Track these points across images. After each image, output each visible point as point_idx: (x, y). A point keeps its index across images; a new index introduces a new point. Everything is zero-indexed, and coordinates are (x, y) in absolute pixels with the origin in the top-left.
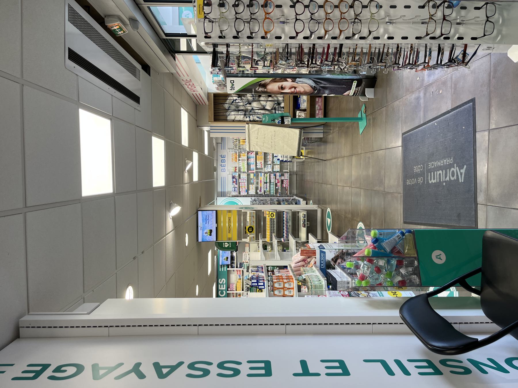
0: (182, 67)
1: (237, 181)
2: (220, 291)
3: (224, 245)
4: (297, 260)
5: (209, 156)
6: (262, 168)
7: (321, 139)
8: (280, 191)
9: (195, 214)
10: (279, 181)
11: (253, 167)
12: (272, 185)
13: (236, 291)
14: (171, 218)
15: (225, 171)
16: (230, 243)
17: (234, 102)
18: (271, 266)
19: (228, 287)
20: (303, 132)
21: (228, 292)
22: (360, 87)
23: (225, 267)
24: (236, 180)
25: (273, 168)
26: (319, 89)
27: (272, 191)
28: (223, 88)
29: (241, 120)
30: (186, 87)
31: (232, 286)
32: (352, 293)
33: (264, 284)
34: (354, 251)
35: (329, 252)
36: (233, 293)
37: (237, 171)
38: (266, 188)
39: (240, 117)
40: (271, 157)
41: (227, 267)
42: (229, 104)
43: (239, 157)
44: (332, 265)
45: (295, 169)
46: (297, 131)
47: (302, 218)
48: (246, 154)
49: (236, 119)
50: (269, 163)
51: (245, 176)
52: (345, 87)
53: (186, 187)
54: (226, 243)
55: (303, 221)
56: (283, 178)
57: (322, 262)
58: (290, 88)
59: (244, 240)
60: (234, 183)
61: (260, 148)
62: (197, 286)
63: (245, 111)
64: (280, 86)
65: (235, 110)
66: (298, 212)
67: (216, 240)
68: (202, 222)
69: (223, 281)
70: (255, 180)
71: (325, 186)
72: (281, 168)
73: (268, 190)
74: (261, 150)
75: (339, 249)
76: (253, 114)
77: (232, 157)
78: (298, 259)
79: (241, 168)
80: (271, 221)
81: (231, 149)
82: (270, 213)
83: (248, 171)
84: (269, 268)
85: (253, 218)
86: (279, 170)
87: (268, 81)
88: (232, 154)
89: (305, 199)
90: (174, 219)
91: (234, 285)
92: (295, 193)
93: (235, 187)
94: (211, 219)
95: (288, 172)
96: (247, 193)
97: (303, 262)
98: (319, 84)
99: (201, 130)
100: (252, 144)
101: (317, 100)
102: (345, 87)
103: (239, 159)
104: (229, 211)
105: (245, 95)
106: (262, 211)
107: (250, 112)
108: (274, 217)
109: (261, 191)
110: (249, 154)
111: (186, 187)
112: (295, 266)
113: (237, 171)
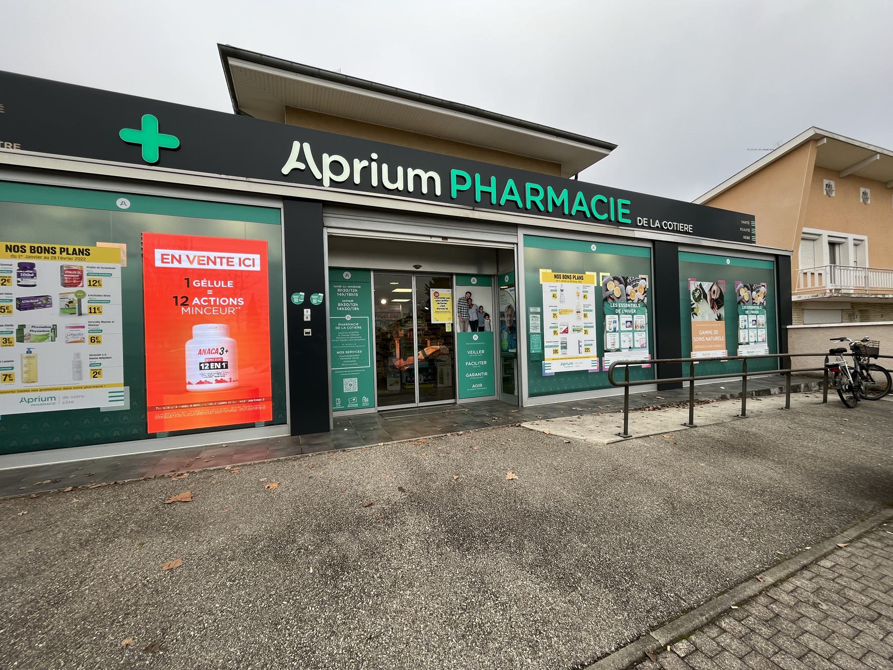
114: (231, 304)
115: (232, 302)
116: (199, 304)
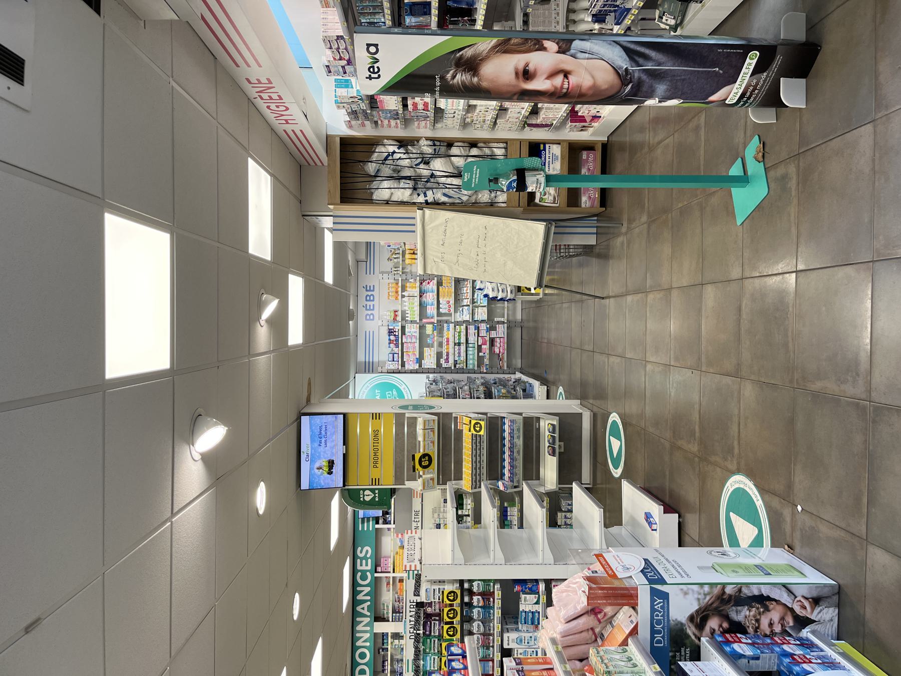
0: (253, 55)
1: (397, 340)
2: (359, 574)
3: (362, 496)
4: (572, 612)
5: (335, 288)
6: (451, 314)
7: (588, 250)
8: (486, 361)
9: (293, 422)
10: (486, 341)
11: (431, 310)
12: (471, 349)
13: (394, 572)
14: (197, 457)
15: (373, 320)
16: (377, 492)
17: (390, 158)
18: (479, 580)
19: (377, 565)
20: (553, 229)
21: (376, 575)
22: (765, 74)
23: (371, 523)
24: (395, 337)
25: (473, 314)
26: (639, 78)
27: (471, 362)
28: (363, 125)
29: (405, 200)
30: (262, 105)
35: (681, 595)
36: (386, 577)
37: (399, 318)
38: (459, 356)
39: (403, 194)
40: (470, 291)
41: (375, 522)
42: (376, 162)
43: (403, 289)
44: (688, 636)
45: (519, 317)
46: (540, 227)
47: (547, 433)
48: (418, 284)
49: (392, 199)
50: (465, 302)
51: (415, 330)
52: (721, 72)
53: (263, 364)
54: (367, 492)
55: (551, 441)
56: (493, 334)
57: (658, 627)
58: (552, 75)
59: (409, 484)
60: (391, 345)
61: (451, 269)
62: (297, 595)
63: (414, 180)
64: (521, 67)
65: (391, 178)
66: (538, 419)
67: (344, 485)
68: (309, 443)
69: (367, 551)
70: (436, 338)
71: (604, 358)
72: (490, 313)
73: (462, 359)
74: (449, 272)
75: (712, 585)
76: (434, 187)
77: (389, 290)
78: (575, 607)
79: (407, 312)
80: (474, 441)
81: (386, 272)
82: (473, 422)
83: (421, 320)
85: (430, 350)
86: (485, 317)
87: (485, 47)
88: (389, 284)
89: (544, 381)
90: (208, 459)
91: (390, 559)
92: (519, 366)
93: (393, 352)
94: (332, 434)
95: (503, 323)
96: (418, 364)
97: (592, 617)
98: (641, 61)
99: (315, 228)
100: (430, 258)
101: (584, 156)
102: (721, 72)
103: (403, 293)
104: (374, 415)
105: (416, 142)
106: (454, 415)
107: (427, 182)
108: (482, 433)
109: (447, 360)
110: (424, 284)
111: (263, 364)
112: (565, 631)
113: (399, 318)
114: (358, 589)
116: (369, 603)
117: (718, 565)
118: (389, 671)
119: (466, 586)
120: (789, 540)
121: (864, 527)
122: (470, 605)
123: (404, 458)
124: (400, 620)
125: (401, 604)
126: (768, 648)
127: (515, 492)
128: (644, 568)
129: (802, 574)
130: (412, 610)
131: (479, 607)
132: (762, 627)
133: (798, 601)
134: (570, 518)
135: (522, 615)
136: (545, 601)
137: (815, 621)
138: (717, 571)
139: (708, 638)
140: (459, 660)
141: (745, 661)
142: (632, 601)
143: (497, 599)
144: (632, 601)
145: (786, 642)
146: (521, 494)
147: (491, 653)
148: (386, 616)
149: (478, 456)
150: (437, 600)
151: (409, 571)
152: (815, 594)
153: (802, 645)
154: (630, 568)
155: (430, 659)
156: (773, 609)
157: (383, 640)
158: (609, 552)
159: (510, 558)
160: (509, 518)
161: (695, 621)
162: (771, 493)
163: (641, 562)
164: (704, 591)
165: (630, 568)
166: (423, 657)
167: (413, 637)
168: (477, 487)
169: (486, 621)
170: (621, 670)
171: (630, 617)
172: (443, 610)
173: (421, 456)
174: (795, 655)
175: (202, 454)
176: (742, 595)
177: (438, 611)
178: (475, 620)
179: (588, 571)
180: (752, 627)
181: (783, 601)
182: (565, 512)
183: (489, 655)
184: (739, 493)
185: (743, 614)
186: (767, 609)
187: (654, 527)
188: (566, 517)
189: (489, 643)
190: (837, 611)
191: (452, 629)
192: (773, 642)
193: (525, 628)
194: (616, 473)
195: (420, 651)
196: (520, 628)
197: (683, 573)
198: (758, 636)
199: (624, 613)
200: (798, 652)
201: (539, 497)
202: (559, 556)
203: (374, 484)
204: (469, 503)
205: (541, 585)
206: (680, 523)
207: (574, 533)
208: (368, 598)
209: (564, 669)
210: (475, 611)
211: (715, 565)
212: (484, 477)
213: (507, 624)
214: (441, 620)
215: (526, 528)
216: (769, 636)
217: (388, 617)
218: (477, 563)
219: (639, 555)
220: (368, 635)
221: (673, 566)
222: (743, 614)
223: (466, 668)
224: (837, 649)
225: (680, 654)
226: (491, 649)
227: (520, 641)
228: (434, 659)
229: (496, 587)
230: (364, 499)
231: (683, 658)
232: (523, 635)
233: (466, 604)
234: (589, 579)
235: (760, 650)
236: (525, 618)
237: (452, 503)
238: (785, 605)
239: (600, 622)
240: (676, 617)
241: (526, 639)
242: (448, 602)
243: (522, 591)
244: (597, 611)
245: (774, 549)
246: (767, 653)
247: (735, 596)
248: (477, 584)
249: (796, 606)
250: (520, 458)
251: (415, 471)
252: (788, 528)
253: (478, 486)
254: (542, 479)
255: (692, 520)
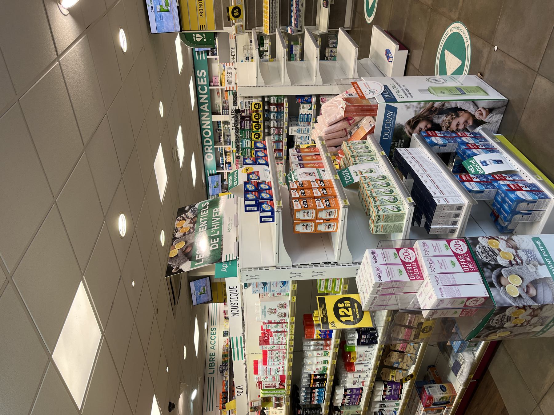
2: (200, 87)
3: (194, 38)
4: (333, 119)
13: (221, 86)
14: (66, 12)
16: (204, 35)
18: (274, 96)
19: (210, 81)
21: (210, 88)
23: (204, 54)
31: (216, 80)
32: (480, 251)
33: (272, 214)
34: (456, 104)
35: (405, 109)
36: (217, 89)
44: (405, 133)
54: (198, 35)
57: (387, 128)
59: (226, 30)
62: (161, 103)
67: (181, 30)
69: (203, 73)
75: (426, 102)
84: (272, 98)
97: (346, 122)
114: (200, 96)
115: (205, 124)
116: (207, 104)
117: (432, 88)
118: (223, 141)
119: (266, 99)
120: (482, 70)
121: (539, 63)
122: (269, 111)
123: (221, 10)
124: (227, 114)
125: (227, 104)
126: (453, 140)
127: (299, 35)
128: (383, 92)
129: (486, 93)
130: (232, 113)
131: (274, 112)
132: (452, 126)
133: (479, 111)
134: (334, 52)
135: (300, 117)
136: (315, 108)
137: (486, 123)
138: (431, 93)
139: (417, 134)
140: (262, 151)
141: (437, 147)
142: (373, 113)
143: (286, 107)
144: (373, 113)
145: (465, 135)
146: (303, 36)
147: (282, 138)
148: (218, 112)
149: (273, 8)
150: (248, 108)
151: (229, 91)
152: (491, 106)
153: (475, 137)
154: (374, 92)
155: (245, 142)
156: (462, 116)
157: (218, 125)
158: (361, 80)
159: (293, 82)
160: (294, 52)
161: (411, 124)
162: (478, 36)
163: (382, 88)
164: (420, 106)
165: (374, 92)
166: (241, 140)
167: (234, 129)
168: (273, 32)
169: (278, 120)
170: (361, 154)
171: (370, 122)
172: (252, 114)
173: (233, 9)
174: (469, 143)
175: (68, 10)
176: (444, 108)
177: (248, 115)
178: (272, 120)
179: (347, 94)
180: (446, 127)
181: (469, 111)
182: (331, 48)
183: (281, 139)
184: (456, 36)
185: (442, 119)
186: (458, 116)
187: (391, 59)
188: (331, 51)
189: (280, 133)
190: (502, 116)
191: (258, 125)
192: (457, 136)
193: (302, 124)
194: (369, 20)
195: (239, 137)
196: (299, 124)
197: (408, 95)
198: (448, 132)
199: (367, 120)
200: (472, 141)
201: (314, 38)
202: (326, 79)
203: (202, 29)
204: (267, 43)
205: (313, 99)
206: (408, 57)
207: (337, 64)
208: (207, 101)
209: (326, 156)
210: (272, 115)
211: (430, 88)
212: (278, 24)
213: (291, 122)
214: (251, 120)
215: (305, 61)
216: (455, 132)
217: (220, 112)
218: (273, 85)
219: (381, 83)
220: (209, 122)
221: (403, 90)
222: (441, 120)
223: (266, 156)
224: (538, 178)
225: (398, 144)
226: (282, 136)
227: (299, 131)
228: (248, 141)
229: (285, 100)
230: (196, 40)
231: (399, 145)
232: (301, 127)
233: (266, 110)
234: (346, 100)
235: (448, 141)
236: (303, 118)
237: (256, 45)
238: (470, 113)
239: (350, 125)
240: (399, 122)
241: (303, 130)
242: (255, 110)
243: (301, 102)
244: (349, 119)
245: (470, 76)
246: (452, 142)
247: (440, 108)
248: (273, 123)
249: (477, 114)
250: (303, 9)
251: (229, 20)
252: (483, 61)
253: (273, 30)
254: (317, 25)
255: (417, 54)
